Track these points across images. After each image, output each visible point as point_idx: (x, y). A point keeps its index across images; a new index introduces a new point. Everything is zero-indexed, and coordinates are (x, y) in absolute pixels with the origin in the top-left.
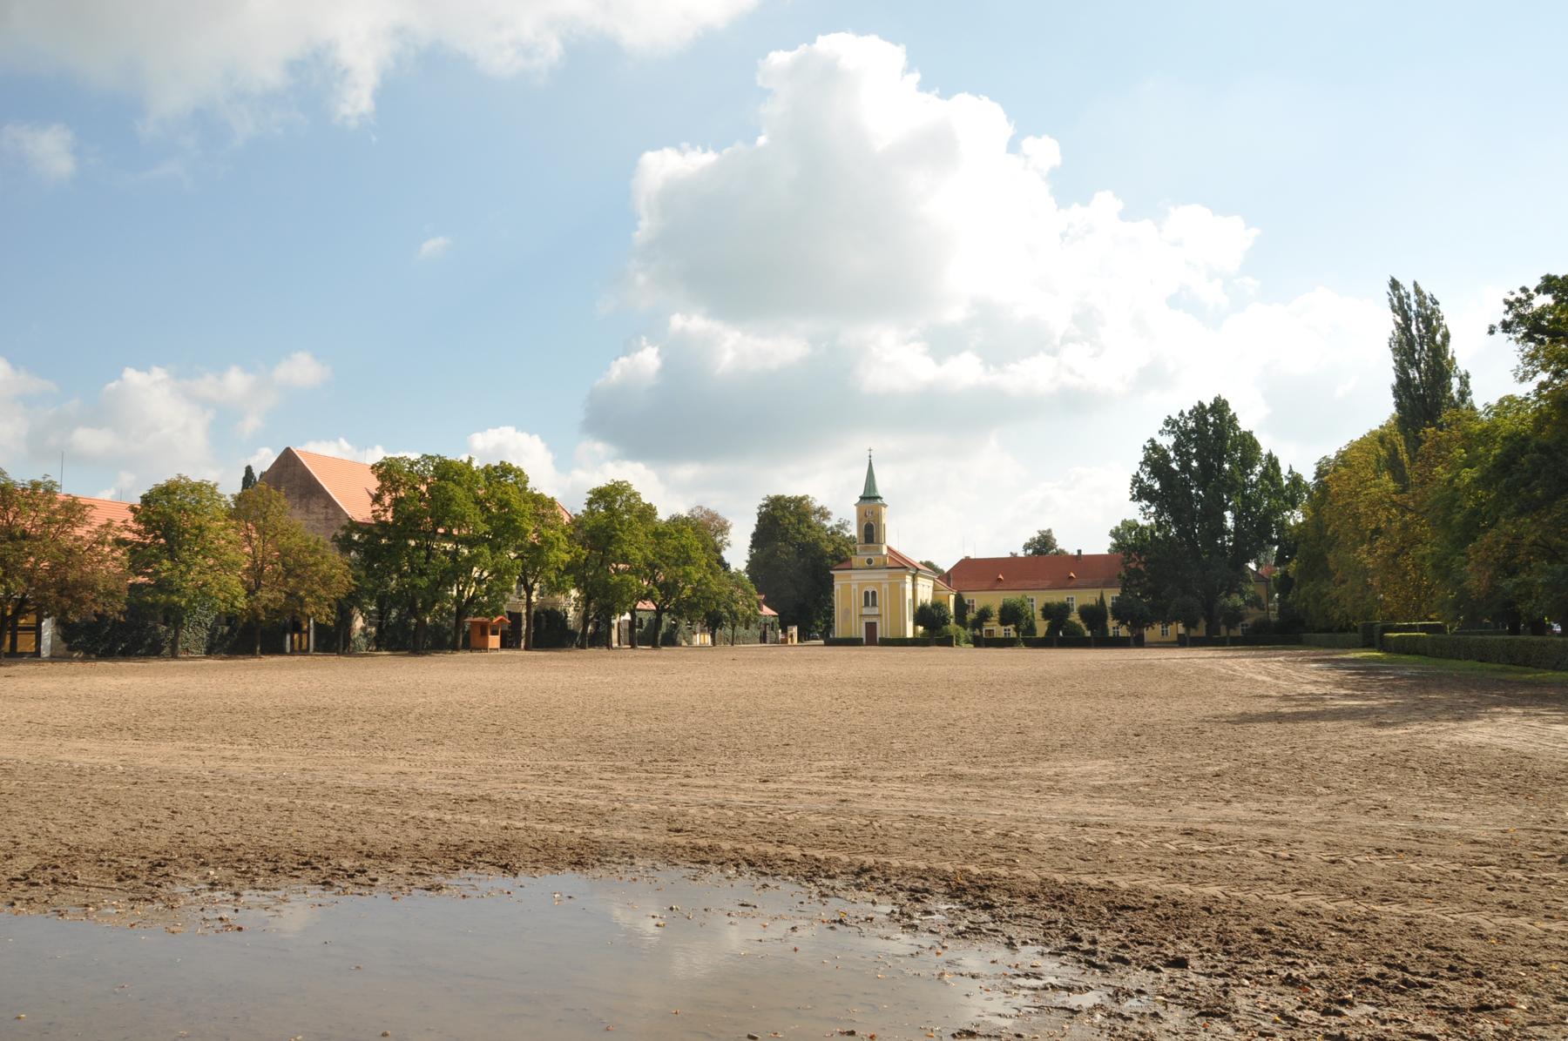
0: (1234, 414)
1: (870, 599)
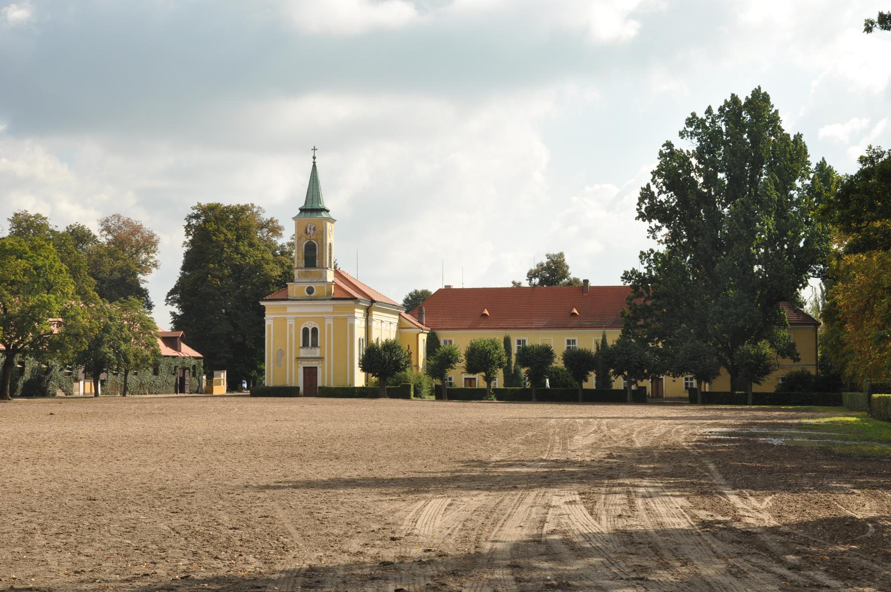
0: (777, 111)
1: (310, 337)
